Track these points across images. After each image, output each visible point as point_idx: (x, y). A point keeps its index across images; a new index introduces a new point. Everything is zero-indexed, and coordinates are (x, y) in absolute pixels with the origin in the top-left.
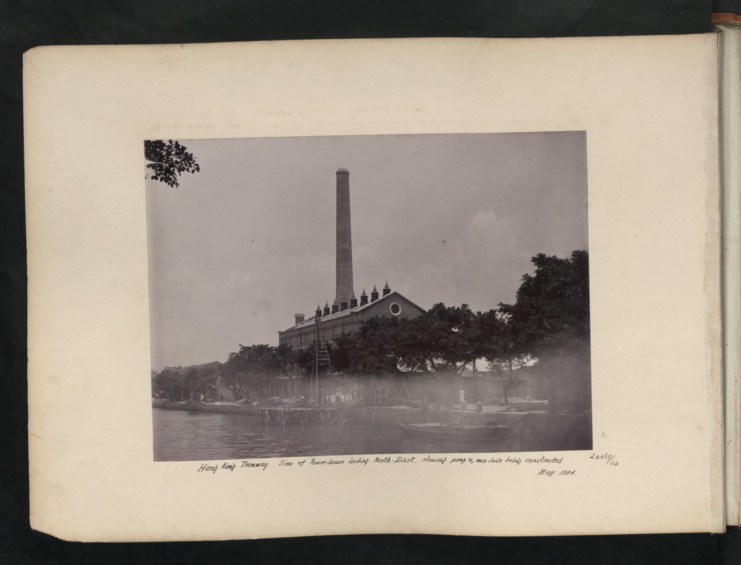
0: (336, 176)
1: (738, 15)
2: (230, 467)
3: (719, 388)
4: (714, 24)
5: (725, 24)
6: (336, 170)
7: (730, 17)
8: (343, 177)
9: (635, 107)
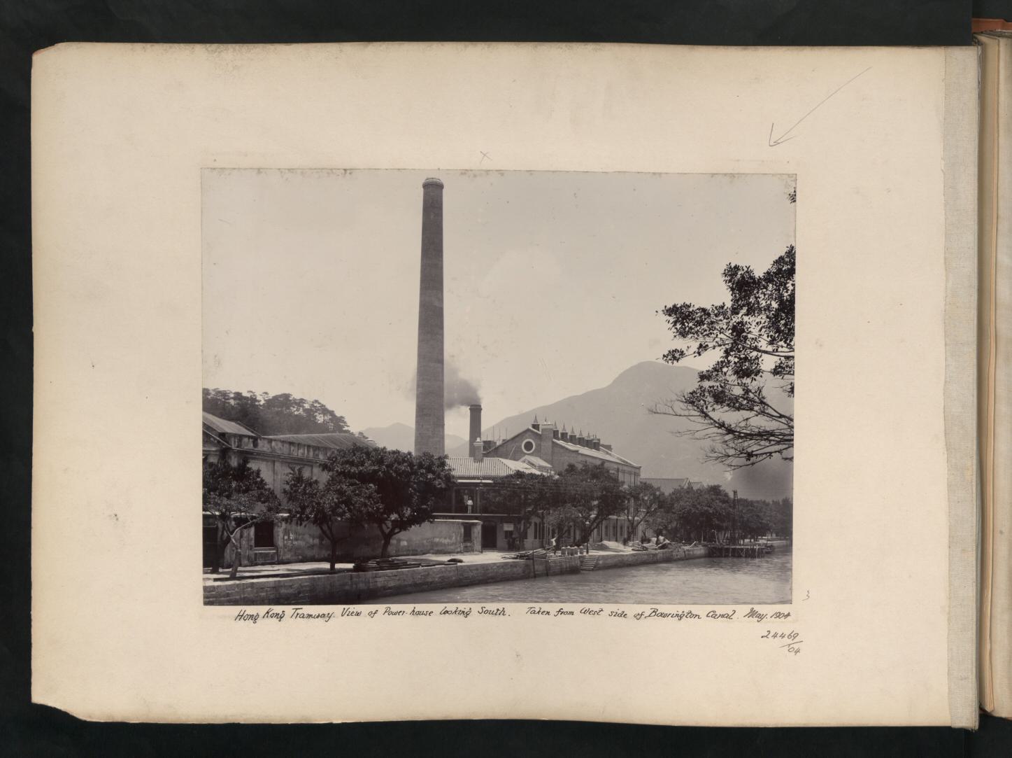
0: (422, 189)
1: (1007, 21)
2: (252, 616)
3: (974, 488)
4: (975, 33)
5: (989, 34)
6: (423, 181)
7: (997, 25)
8: (433, 195)
9: (857, 146)
